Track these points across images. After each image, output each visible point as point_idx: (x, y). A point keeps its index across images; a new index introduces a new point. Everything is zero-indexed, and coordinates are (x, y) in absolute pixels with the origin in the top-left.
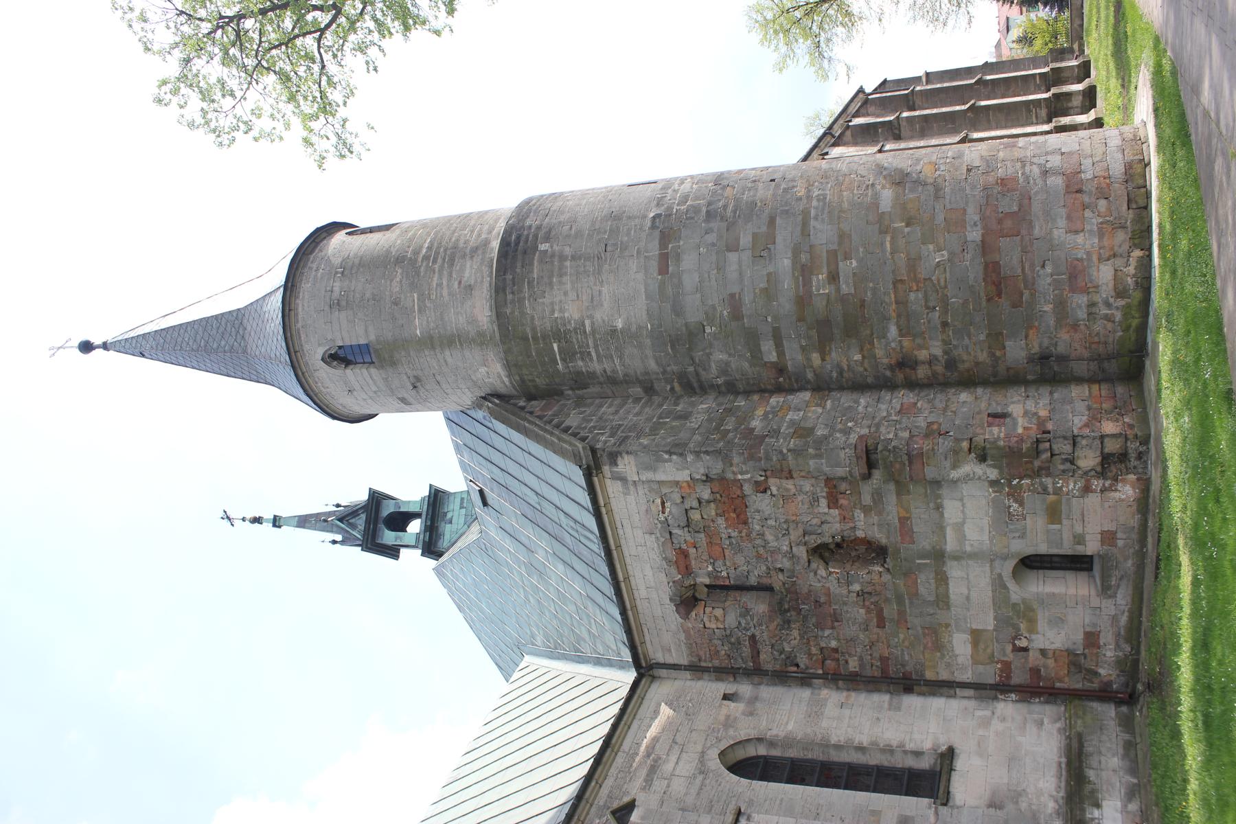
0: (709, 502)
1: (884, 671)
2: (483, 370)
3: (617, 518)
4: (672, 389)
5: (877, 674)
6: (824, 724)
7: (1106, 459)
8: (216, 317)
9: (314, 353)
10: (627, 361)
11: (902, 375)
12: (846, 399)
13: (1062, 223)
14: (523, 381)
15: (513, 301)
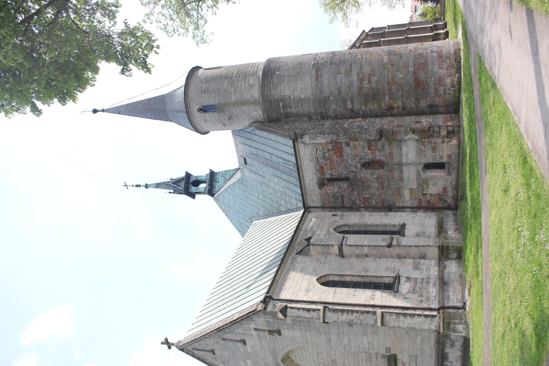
0: (331, 150)
1: (383, 204)
2: (255, 113)
3: (301, 156)
4: (317, 118)
5: (381, 205)
6: (365, 220)
7: (449, 132)
8: (153, 98)
9: (195, 108)
10: (304, 108)
11: (389, 112)
12: (372, 120)
13: (436, 66)
14: (268, 116)
15: (267, 90)
